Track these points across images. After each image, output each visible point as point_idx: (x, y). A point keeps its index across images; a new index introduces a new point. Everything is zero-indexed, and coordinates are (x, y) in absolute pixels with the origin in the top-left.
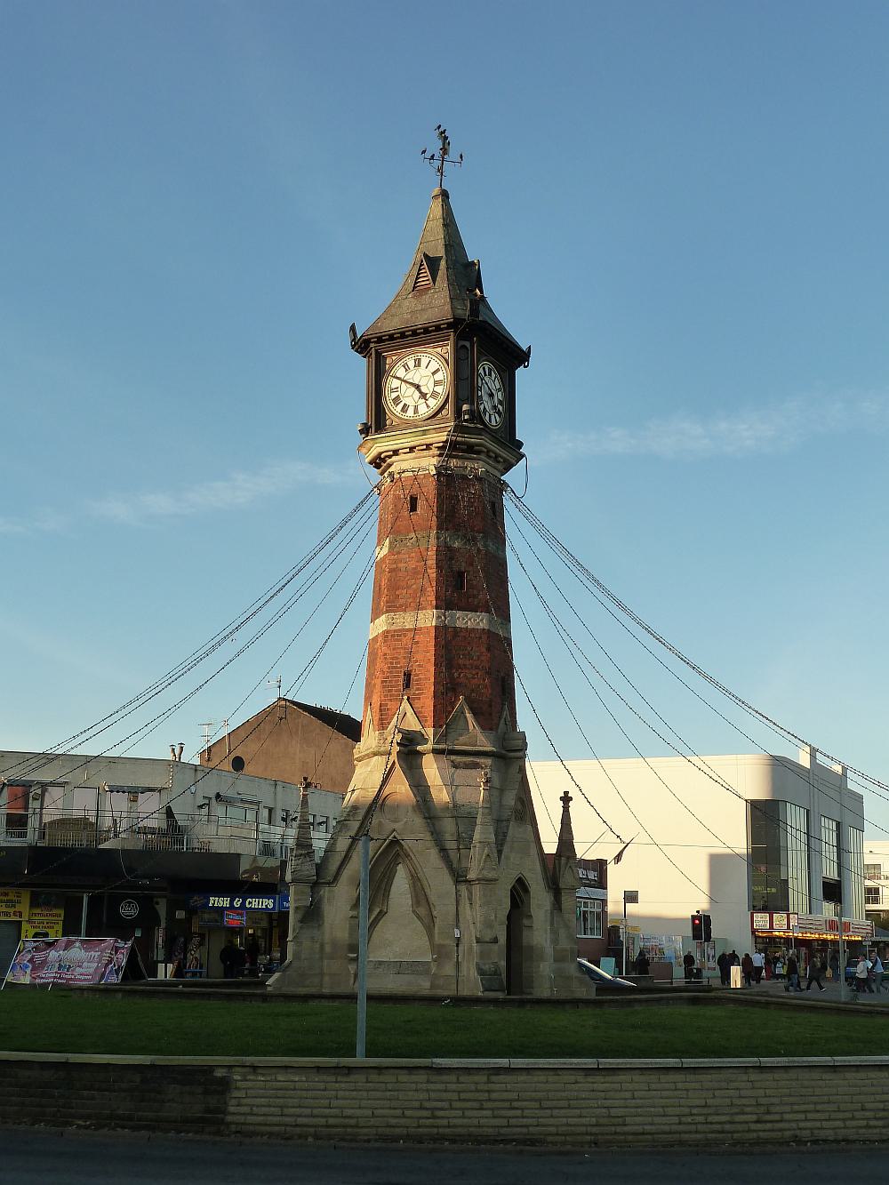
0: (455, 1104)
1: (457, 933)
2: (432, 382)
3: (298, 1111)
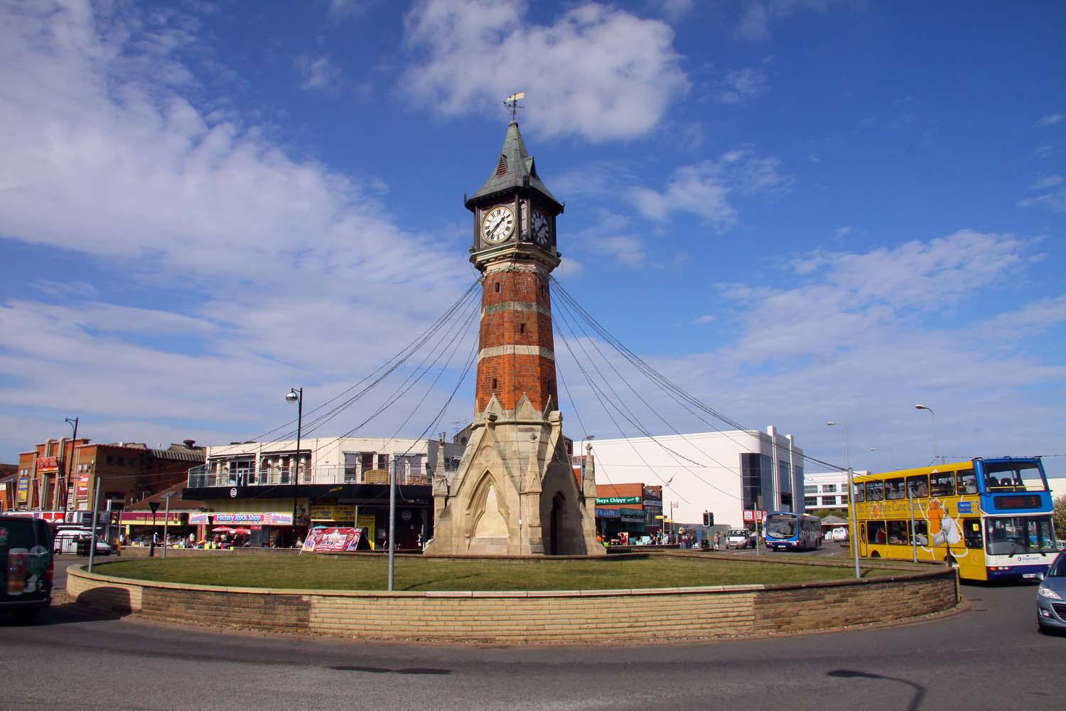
0: (440, 618)
1: (520, 522)
3: (348, 621)
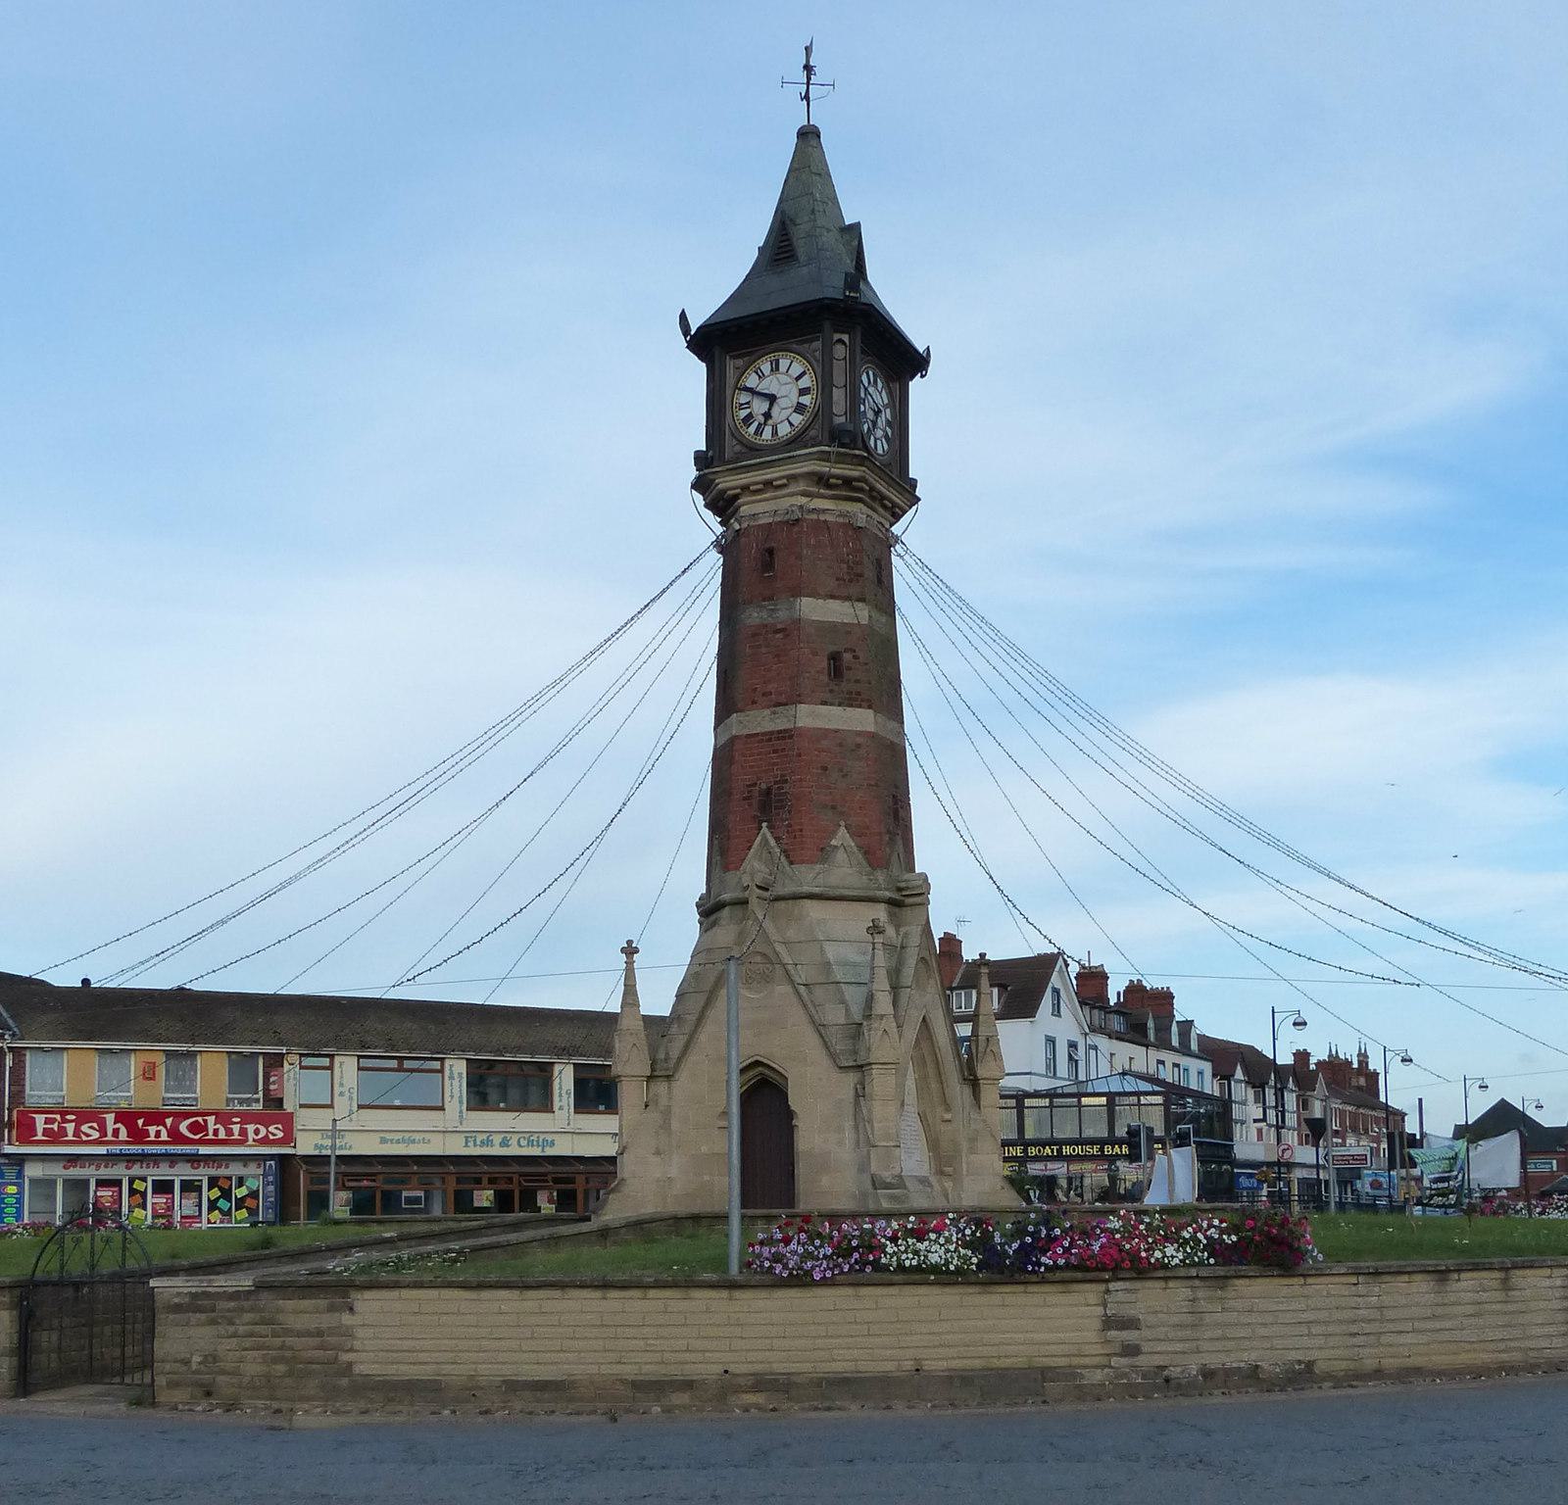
2: (795, 392)
